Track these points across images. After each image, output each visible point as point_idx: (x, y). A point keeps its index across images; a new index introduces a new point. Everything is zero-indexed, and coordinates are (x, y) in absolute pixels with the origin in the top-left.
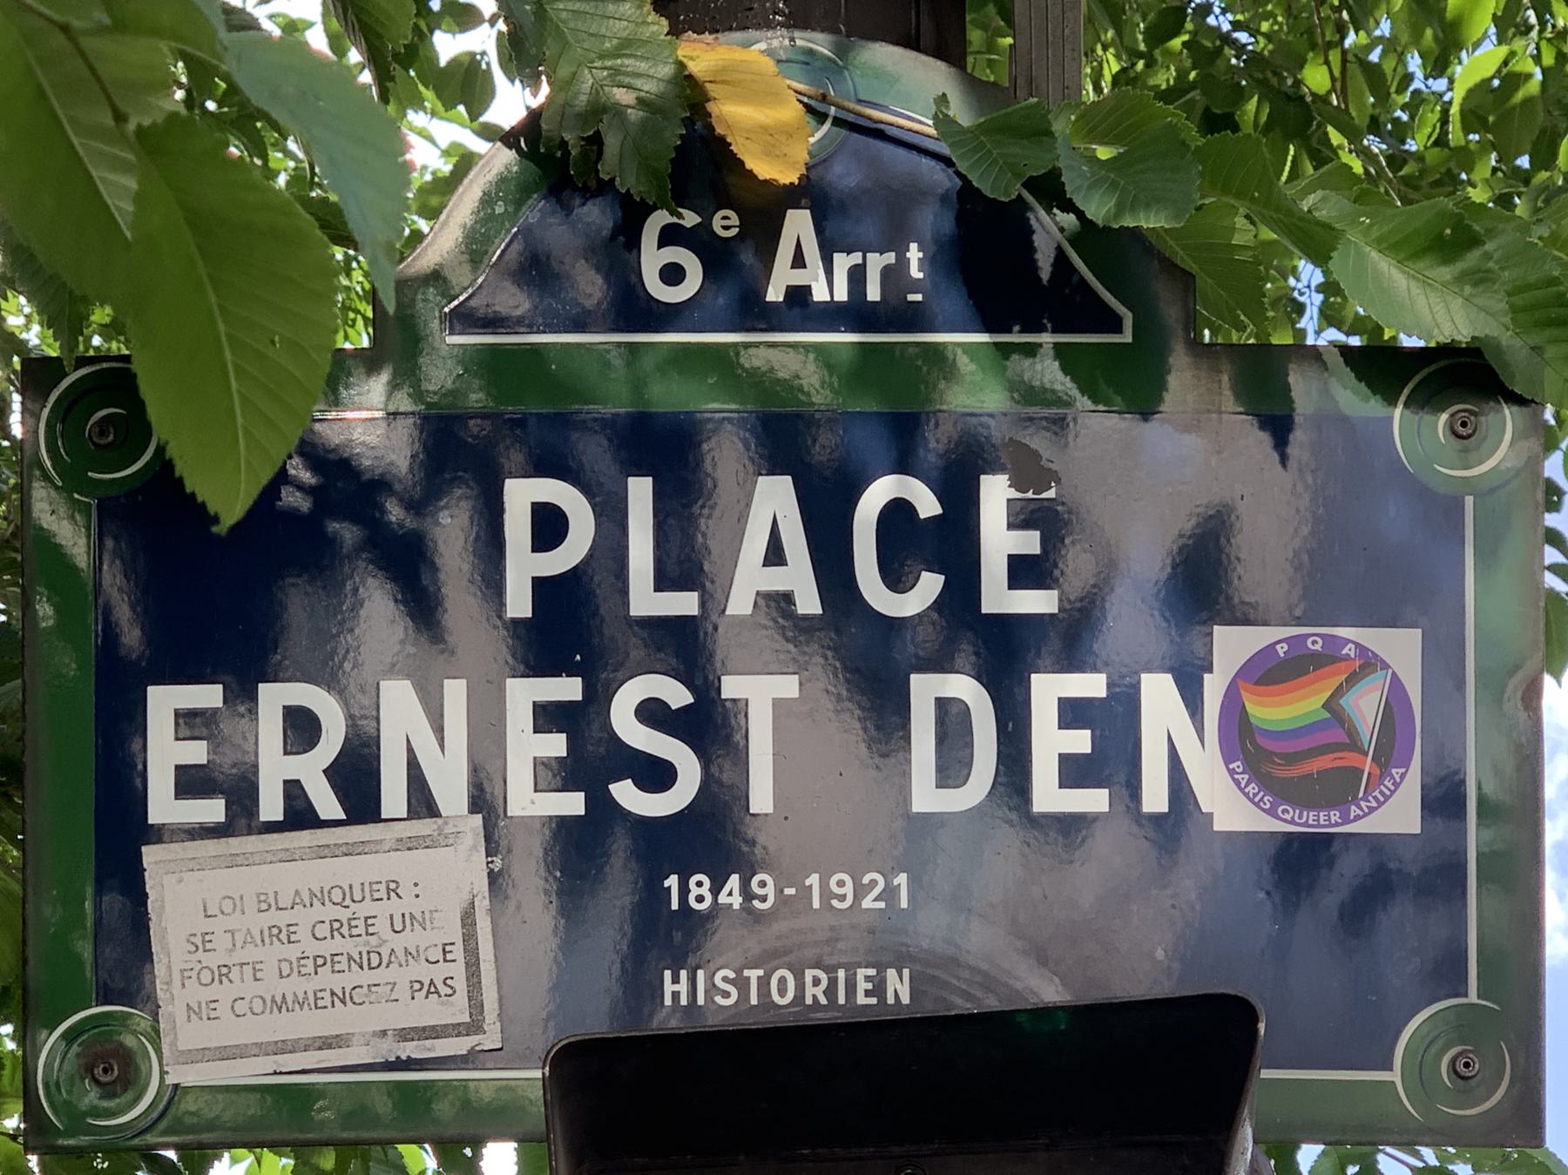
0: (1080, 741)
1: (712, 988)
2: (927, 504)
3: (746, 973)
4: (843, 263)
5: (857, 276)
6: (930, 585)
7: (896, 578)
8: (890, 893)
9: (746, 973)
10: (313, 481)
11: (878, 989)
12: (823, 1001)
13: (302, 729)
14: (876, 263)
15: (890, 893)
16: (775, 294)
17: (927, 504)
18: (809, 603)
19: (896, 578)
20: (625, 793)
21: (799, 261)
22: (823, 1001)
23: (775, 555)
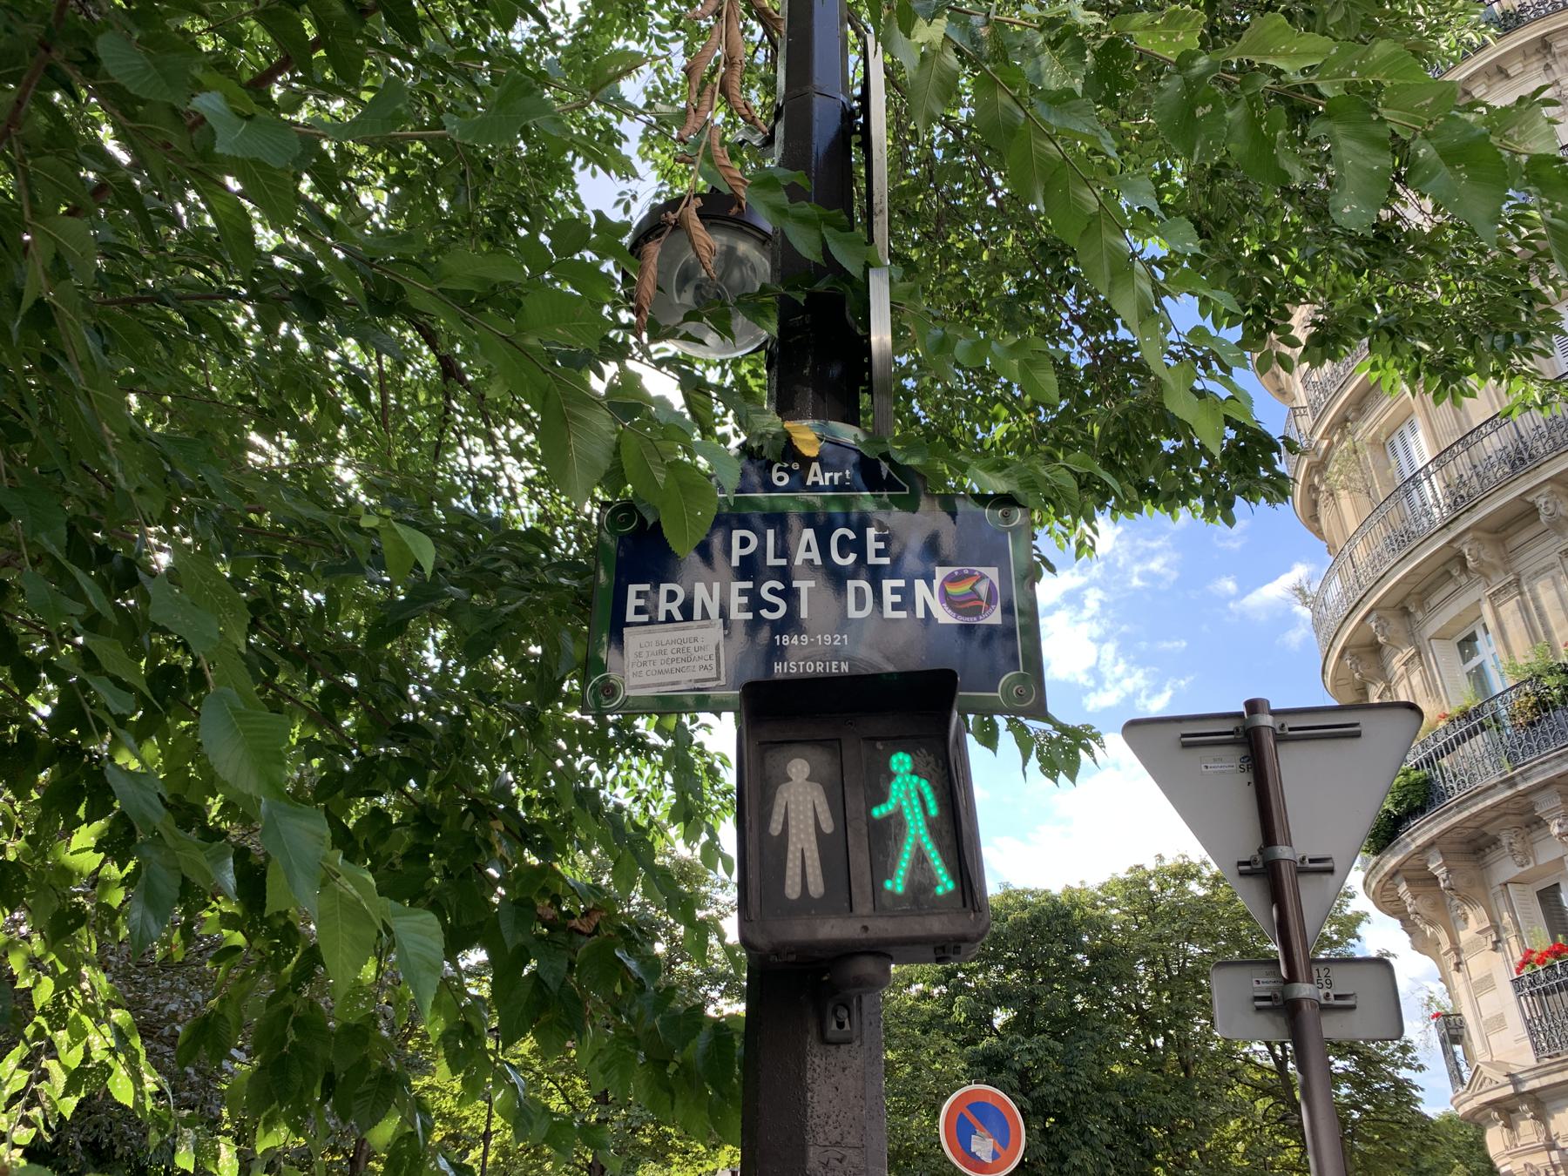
0: (898, 598)
2: (852, 536)
4: (827, 475)
5: (832, 479)
6: (852, 557)
7: (843, 555)
8: (842, 641)
10: (901, 762)
11: (839, 668)
14: (837, 476)
15: (842, 641)
16: (809, 483)
17: (852, 536)
18: (818, 562)
19: (843, 555)
21: (808, 549)
23: (808, 549)
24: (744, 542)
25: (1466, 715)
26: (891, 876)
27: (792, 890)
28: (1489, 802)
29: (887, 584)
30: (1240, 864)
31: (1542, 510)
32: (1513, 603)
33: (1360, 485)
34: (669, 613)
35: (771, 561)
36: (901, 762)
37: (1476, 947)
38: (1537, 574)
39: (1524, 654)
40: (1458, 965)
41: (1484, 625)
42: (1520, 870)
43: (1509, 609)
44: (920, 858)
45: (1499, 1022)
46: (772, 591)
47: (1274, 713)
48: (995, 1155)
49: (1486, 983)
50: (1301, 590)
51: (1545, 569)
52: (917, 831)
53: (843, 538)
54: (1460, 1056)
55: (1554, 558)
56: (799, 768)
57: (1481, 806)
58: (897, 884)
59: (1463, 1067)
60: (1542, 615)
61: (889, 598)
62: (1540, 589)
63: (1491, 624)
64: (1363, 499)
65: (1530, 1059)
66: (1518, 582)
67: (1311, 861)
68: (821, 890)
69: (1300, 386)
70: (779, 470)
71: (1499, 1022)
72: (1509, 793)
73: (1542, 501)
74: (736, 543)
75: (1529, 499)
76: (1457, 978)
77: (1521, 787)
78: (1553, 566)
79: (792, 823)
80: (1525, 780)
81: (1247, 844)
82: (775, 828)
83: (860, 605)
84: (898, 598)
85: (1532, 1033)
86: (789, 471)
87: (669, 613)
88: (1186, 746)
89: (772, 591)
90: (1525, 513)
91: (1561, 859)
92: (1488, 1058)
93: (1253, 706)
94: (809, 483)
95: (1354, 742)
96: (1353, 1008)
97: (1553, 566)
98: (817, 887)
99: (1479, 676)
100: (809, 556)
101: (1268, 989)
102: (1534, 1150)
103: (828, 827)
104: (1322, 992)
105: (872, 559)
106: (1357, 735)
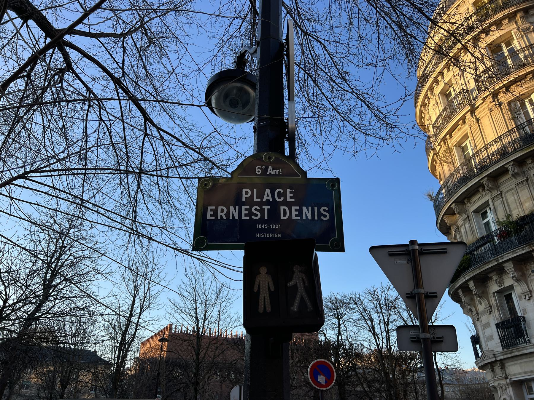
0: (297, 213)
1: (320, 214)
2: (282, 191)
3: (263, 207)
4: (274, 171)
5: (276, 172)
6: (282, 198)
7: (279, 198)
8: (279, 227)
9: (263, 207)
10: (297, 269)
11: (278, 235)
12: (225, 218)
13: (222, 211)
14: (277, 171)
15: (279, 227)
16: (268, 173)
17: (282, 191)
18: (271, 200)
19: (279, 198)
20: (253, 217)
21: (268, 196)
22: (225, 218)
23: (268, 196)
24: (247, 193)
25: (482, 238)
26: (293, 305)
27: (261, 309)
28: (490, 266)
29: (294, 208)
30: (407, 294)
31: (510, 170)
32: (499, 201)
33: (451, 161)
34: (221, 216)
35: (255, 199)
36: (297, 269)
37: (483, 313)
38: (508, 191)
39: (502, 217)
40: (478, 319)
41: (490, 208)
42: (499, 288)
43: (498, 202)
44: (302, 298)
45: (491, 338)
46: (256, 210)
47: (420, 245)
48: (326, 382)
49: (487, 325)
50: (430, 195)
51: (510, 190)
52: (301, 291)
53: (279, 192)
54: (478, 348)
55: (514, 186)
56: (263, 270)
57: (487, 267)
58: (295, 308)
59: (479, 352)
60: (508, 205)
61: (294, 213)
62: (508, 197)
63: (492, 208)
64: (452, 166)
65: (500, 349)
66: (501, 193)
67: (430, 293)
68: (270, 310)
69: (432, 128)
70: (258, 168)
71: (491, 338)
72: (496, 263)
73: (510, 167)
74: (244, 193)
75: (506, 167)
76: (478, 323)
77: (500, 261)
78: (513, 189)
79: (261, 287)
80: (502, 259)
81: (409, 287)
82: (256, 290)
83: (285, 215)
84: (297, 213)
85: (501, 341)
86: (261, 169)
87: (221, 216)
88: (390, 255)
89: (256, 210)
90: (503, 171)
91: (512, 285)
92: (487, 349)
93: (413, 242)
94: (268, 173)
95: (445, 255)
96: (442, 341)
97: (513, 189)
98: (269, 309)
99: (487, 224)
100: (268, 198)
101: (415, 335)
102: (501, 379)
103: (272, 289)
104: (432, 336)
105: (289, 200)
106: (446, 252)
